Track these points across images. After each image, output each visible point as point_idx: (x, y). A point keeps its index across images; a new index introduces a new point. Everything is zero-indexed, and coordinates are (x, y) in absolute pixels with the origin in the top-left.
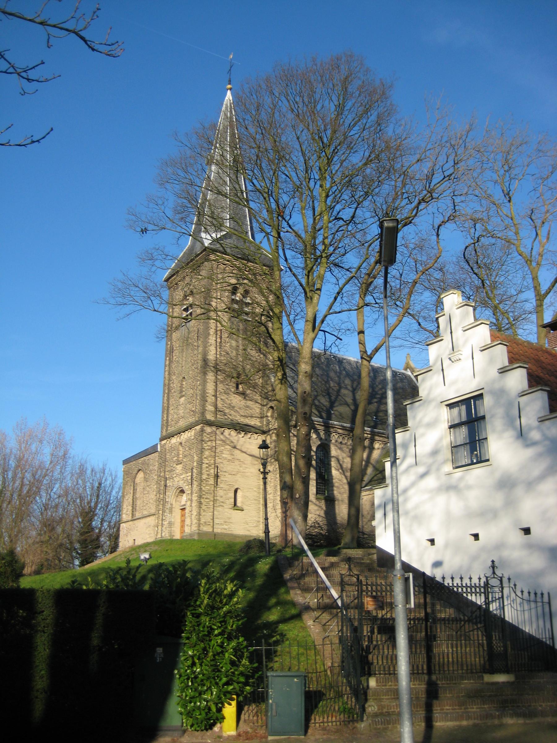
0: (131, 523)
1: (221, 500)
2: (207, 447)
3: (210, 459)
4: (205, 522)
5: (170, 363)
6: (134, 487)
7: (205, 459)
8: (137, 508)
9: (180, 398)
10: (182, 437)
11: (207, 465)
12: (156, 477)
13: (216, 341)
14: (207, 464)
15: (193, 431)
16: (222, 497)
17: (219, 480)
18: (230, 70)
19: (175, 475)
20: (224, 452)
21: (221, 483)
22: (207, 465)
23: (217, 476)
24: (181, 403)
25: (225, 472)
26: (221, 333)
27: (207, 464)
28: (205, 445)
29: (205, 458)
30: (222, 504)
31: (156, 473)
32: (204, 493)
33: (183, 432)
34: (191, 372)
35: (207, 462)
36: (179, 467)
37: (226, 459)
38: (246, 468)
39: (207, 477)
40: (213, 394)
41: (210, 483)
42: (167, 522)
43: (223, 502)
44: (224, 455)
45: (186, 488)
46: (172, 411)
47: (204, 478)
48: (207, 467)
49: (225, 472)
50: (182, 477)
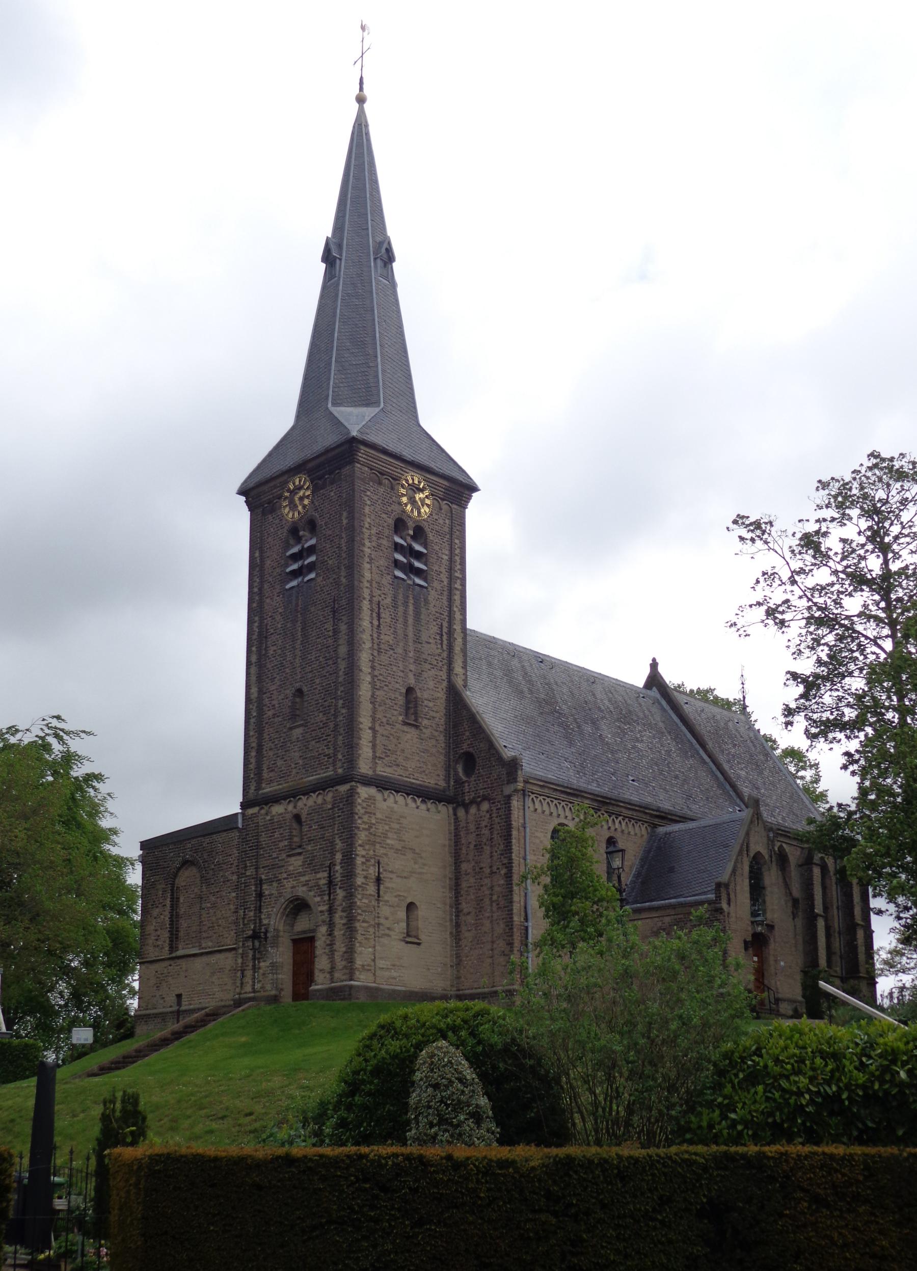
0: (166, 963)
1: (387, 924)
2: (363, 826)
3: (367, 847)
4: (363, 966)
5: (259, 659)
6: (172, 895)
7: (359, 848)
8: (181, 934)
9: (291, 729)
10: (300, 804)
11: (364, 860)
12: (235, 878)
13: (371, 623)
14: (363, 856)
15: (331, 795)
16: (387, 919)
17: (382, 887)
18: (784, 558)
19: (285, 875)
20: (390, 835)
21: (385, 892)
22: (364, 860)
23: (378, 880)
24: (294, 738)
25: (392, 872)
26: (379, 608)
27: (363, 856)
28: (359, 821)
29: (360, 846)
30: (387, 932)
31: (234, 869)
32: (359, 911)
33: (304, 795)
34: (317, 681)
35: (364, 853)
36: (296, 863)
37: (391, 847)
38: (425, 865)
39: (363, 880)
40: (370, 725)
41: (368, 893)
42: (268, 964)
43: (389, 929)
44: (389, 841)
45: (314, 899)
46: (271, 753)
47: (359, 883)
48: (363, 863)
49: (392, 872)
50: (303, 879)
